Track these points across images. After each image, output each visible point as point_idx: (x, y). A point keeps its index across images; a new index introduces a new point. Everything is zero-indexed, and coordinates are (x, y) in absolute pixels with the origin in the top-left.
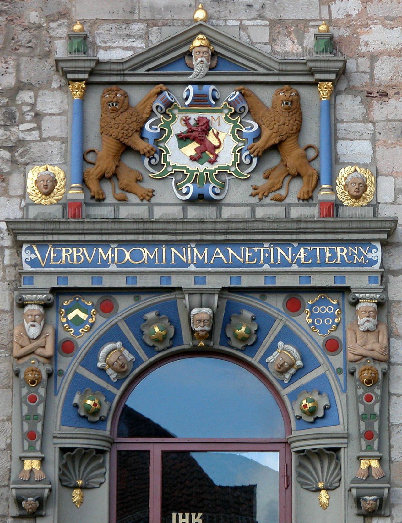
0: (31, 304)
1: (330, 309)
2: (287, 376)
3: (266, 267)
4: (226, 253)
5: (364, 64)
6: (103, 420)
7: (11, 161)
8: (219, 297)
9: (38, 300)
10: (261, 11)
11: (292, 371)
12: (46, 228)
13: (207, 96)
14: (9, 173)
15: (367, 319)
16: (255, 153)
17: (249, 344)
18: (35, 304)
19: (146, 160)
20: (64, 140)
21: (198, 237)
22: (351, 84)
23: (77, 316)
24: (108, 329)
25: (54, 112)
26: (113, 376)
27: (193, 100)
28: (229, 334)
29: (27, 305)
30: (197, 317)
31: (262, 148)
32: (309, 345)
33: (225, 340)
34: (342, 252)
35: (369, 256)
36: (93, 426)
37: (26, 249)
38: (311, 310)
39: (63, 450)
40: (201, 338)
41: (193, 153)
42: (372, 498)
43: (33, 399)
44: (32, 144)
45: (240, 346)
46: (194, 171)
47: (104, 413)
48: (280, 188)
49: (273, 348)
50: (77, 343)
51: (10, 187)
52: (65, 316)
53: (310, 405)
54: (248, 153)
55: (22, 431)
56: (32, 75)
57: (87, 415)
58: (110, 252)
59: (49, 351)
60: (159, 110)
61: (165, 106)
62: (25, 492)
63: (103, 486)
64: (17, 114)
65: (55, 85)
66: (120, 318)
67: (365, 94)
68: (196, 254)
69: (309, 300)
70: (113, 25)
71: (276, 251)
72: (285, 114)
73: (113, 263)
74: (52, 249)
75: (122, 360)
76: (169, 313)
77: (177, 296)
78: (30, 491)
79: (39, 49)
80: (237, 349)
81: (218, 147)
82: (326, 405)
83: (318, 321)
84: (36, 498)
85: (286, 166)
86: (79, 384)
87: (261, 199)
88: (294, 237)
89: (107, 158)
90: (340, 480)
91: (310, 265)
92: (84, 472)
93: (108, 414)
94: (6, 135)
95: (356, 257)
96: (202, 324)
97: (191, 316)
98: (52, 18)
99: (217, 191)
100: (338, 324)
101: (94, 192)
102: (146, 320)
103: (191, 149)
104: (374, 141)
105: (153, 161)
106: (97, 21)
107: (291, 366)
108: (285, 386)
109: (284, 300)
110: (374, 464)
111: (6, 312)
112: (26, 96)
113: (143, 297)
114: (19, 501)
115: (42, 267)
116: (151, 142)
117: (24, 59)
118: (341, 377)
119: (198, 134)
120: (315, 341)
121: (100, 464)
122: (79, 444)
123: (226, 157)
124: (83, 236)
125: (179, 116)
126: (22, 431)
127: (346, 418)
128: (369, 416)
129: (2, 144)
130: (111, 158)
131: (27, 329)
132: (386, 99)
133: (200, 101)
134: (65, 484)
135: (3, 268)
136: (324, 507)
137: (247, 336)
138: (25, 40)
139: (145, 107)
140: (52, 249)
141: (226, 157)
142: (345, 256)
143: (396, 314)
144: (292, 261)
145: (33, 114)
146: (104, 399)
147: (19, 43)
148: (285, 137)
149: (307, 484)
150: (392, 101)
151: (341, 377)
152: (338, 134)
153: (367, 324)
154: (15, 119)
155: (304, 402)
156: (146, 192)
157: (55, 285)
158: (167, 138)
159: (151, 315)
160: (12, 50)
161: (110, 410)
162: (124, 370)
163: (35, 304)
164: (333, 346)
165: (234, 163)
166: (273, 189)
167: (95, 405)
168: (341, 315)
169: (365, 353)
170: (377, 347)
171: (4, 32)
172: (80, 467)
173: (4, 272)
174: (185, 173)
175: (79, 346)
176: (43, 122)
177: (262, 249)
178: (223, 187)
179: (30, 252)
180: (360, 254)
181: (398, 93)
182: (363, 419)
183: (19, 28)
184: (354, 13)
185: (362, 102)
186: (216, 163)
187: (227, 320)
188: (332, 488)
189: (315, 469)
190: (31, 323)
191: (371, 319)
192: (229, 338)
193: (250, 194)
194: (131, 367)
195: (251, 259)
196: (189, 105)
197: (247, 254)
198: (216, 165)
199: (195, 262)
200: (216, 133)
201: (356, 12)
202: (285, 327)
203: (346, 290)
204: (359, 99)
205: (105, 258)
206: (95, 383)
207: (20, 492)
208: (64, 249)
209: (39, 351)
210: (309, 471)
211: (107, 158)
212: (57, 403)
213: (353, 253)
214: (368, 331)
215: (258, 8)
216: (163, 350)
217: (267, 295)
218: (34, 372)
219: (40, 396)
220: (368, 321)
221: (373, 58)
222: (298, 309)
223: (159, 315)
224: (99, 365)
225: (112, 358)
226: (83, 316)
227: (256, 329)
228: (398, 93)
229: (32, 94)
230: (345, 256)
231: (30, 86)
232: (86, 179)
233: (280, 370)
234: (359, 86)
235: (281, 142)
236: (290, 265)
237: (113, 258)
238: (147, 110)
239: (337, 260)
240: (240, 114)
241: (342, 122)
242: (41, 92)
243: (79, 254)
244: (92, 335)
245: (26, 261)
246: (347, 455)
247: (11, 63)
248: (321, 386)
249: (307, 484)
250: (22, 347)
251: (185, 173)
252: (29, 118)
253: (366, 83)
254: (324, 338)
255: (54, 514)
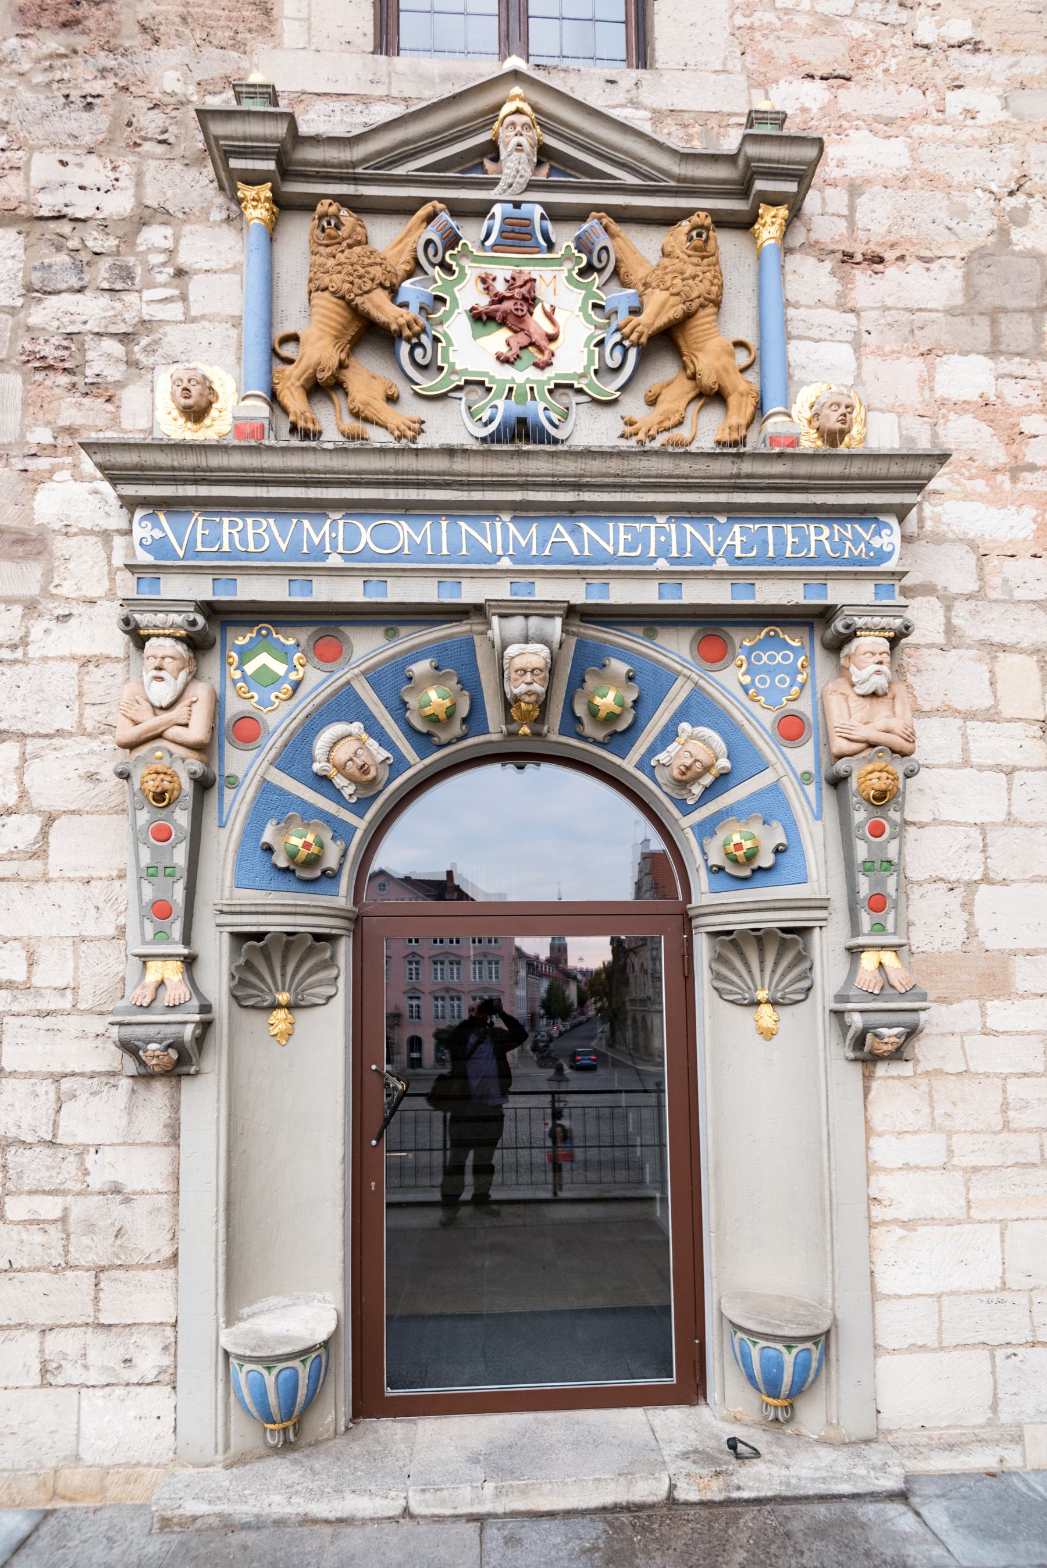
0: (158, 636)
1: (785, 657)
2: (697, 790)
3: (662, 564)
4: (575, 532)
5: (837, 200)
6: (331, 876)
7: (127, 362)
8: (564, 624)
9: (171, 627)
10: (634, 92)
11: (707, 780)
12: (176, 464)
13: (530, 220)
14: (119, 384)
15: (878, 667)
16: (634, 337)
17: (620, 729)
18: (165, 636)
19: (404, 348)
20: (237, 322)
21: (517, 496)
22: (813, 236)
23: (264, 666)
24: (331, 695)
25: (215, 267)
26: (348, 790)
27: (502, 232)
28: (580, 710)
29: (148, 637)
30: (518, 663)
31: (649, 326)
32: (746, 723)
33: (571, 723)
34: (820, 536)
35: (876, 542)
36: (308, 888)
37: (143, 518)
38: (748, 658)
39: (240, 938)
40: (525, 717)
41: (504, 349)
42: (896, 1031)
43: (163, 835)
44: (168, 329)
45: (600, 735)
46: (507, 381)
47: (331, 861)
48: (680, 423)
49: (668, 735)
50: (264, 722)
51: (123, 412)
52: (240, 667)
53: (747, 845)
54: (617, 337)
55: (141, 900)
56: (169, 194)
57: (292, 867)
58: (326, 528)
59: (197, 732)
60: (431, 251)
61: (442, 239)
62: (140, 1031)
63: (332, 1001)
64: (138, 271)
65: (217, 215)
66: (356, 671)
67: (839, 256)
68: (514, 537)
69: (743, 639)
70: (336, 104)
71: (681, 532)
72: (695, 260)
73: (341, 554)
74: (201, 519)
75: (363, 758)
76: (459, 666)
77: (475, 628)
78: (152, 1030)
79: (183, 146)
80: (595, 742)
81: (552, 338)
82: (781, 844)
83: (763, 681)
84: (165, 1043)
85: (693, 377)
86: (270, 803)
87: (641, 443)
88: (723, 498)
89: (320, 338)
90: (809, 989)
91: (753, 561)
92: (294, 975)
93: (341, 865)
94: (113, 308)
95: (848, 544)
96: (528, 677)
97: (505, 661)
98: (210, 88)
99: (555, 418)
100: (803, 686)
101: (295, 413)
102: (410, 679)
103: (499, 339)
104: (857, 346)
105: (418, 352)
106: (303, 97)
107: (707, 769)
108: (686, 810)
109: (694, 637)
110: (889, 958)
111: (117, 660)
112: (155, 236)
113: (404, 631)
114: (129, 1048)
115: (179, 559)
116: (413, 311)
117: (153, 164)
118: (811, 789)
119: (508, 311)
120: (758, 721)
121: (326, 961)
122: (274, 924)
123: (572, 357)
124: (265, 489)
125: (472, 271)
126: (141, 900)
127: (820, 873)
128: (877, 865)
129: (106, 327)
130: (327, 340)
131: (146, 685)
132: (879, 267)
133: (516, 235)
134: (250, 1003)
135: (110, 572)
136: (768, 1034)
137: (617, 710)
138: (153, 125)
139: (401, 252)
140: (201, 519)
141: (572, 357)
142: (827, 543)
143: (913, 669)
144: (716, 552)
145: (171, 271)
146: (331, 835)
147: (143, 133)
148: (695, 304)
149: (731, 993)
150: (892, 271)
151: (811, 789)
152: (790, 329)
153: (876, 677)
154: (133, 279)
155: (736, 838)
156: (408, 423)
157: (209, 597)
158: (448, 314)
159: (421, 668)
160: (128, 146)
161: (344, 856)
162: (370, 777)
163: (165, 636)
164: (791, 728)
165: (587, 368)
166: (667, 424)
167: (307, 845)
168: (808, 670)
169: (874, 735)
170: (897, 725)
171: (111, 109)
172: (284, 967)
173: (112, 580)
174: (487, 385)
175: (271, 729)
176: (191, 286)
177: (653, 526)
178: (566, 414)
179: (150, 525)
180: (857, 540)
181: (902, 258)
182: (866, 871)
183: (144, 104)
184: (815, 107)
185: (833, 273)
186: (548, 369)
187: (577, 682)
188: (786, 1001)
189: (746, 964)
190: (155, 673)
191: (884, 668)
192: (579, 720)
193: (620, 433)
194: (384, 775)
195: (629, 547)
196: (494, 248)
197: (622, 537)
198: (550, 372)
199: (511, 552)
200: (548, 309)
201: (819, 105)
202: (697, 689)
203: (826, 614)
204: (828, 265)
205: (316, 540)
206: (310, 805)
207: (127, 1031)
208: (226, 520)
209: (174, 732)
210: (733, 969)
211: (320, 338)
212: (223, 840)
213: (843, 539)
214: (874, 695)
215: (628, 87)
216: (449, 743)
217: (658, 628)
218: (162, 776)
219: (179, 827)
220: (878, 672)
221: (854, 190)
222: (713, 662)
223: (436, 668)
224: (316, 767)
225: (342, 753)
226: (279, 668)
227: (635, 697)
228: (902, 258)
229: (169, 231)
230: (827, 543)
231: (166, 217)
232: (279, 387)
233: (684, 778)
234: (828, 240)
235: (688, 316)
236: (713, 560)
237: (334, 541)
238: (407, 256)
239: (809, 551)
240: (600, 271)
241: (796, 306)
242: (187, 229)
243: (260, 531)
244: (297, 706)
245: (141, 544)
246: (827, 947)
247: (125, 169)
248: (771, 806)
249: (731, 993)
250: (136, 723)
251: (487, 385)
252: (162, 278)
253: (841, 235)
254: (774, 714)
255: (219, 1070)
